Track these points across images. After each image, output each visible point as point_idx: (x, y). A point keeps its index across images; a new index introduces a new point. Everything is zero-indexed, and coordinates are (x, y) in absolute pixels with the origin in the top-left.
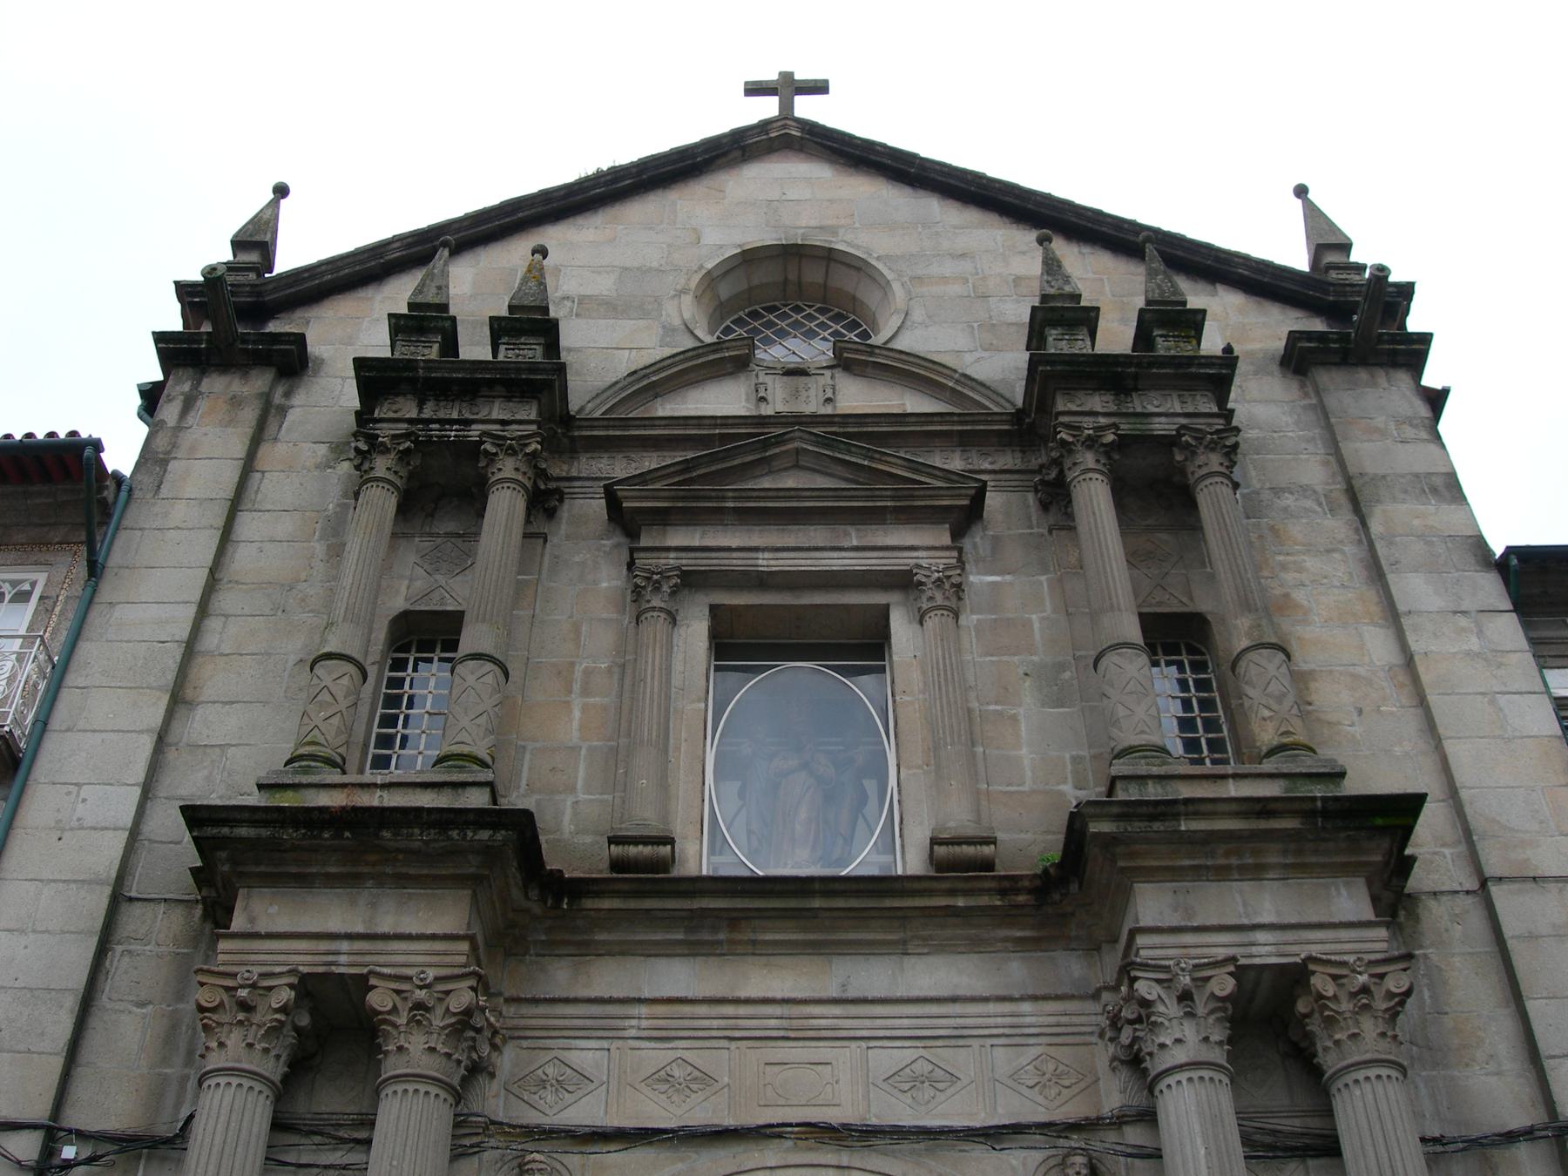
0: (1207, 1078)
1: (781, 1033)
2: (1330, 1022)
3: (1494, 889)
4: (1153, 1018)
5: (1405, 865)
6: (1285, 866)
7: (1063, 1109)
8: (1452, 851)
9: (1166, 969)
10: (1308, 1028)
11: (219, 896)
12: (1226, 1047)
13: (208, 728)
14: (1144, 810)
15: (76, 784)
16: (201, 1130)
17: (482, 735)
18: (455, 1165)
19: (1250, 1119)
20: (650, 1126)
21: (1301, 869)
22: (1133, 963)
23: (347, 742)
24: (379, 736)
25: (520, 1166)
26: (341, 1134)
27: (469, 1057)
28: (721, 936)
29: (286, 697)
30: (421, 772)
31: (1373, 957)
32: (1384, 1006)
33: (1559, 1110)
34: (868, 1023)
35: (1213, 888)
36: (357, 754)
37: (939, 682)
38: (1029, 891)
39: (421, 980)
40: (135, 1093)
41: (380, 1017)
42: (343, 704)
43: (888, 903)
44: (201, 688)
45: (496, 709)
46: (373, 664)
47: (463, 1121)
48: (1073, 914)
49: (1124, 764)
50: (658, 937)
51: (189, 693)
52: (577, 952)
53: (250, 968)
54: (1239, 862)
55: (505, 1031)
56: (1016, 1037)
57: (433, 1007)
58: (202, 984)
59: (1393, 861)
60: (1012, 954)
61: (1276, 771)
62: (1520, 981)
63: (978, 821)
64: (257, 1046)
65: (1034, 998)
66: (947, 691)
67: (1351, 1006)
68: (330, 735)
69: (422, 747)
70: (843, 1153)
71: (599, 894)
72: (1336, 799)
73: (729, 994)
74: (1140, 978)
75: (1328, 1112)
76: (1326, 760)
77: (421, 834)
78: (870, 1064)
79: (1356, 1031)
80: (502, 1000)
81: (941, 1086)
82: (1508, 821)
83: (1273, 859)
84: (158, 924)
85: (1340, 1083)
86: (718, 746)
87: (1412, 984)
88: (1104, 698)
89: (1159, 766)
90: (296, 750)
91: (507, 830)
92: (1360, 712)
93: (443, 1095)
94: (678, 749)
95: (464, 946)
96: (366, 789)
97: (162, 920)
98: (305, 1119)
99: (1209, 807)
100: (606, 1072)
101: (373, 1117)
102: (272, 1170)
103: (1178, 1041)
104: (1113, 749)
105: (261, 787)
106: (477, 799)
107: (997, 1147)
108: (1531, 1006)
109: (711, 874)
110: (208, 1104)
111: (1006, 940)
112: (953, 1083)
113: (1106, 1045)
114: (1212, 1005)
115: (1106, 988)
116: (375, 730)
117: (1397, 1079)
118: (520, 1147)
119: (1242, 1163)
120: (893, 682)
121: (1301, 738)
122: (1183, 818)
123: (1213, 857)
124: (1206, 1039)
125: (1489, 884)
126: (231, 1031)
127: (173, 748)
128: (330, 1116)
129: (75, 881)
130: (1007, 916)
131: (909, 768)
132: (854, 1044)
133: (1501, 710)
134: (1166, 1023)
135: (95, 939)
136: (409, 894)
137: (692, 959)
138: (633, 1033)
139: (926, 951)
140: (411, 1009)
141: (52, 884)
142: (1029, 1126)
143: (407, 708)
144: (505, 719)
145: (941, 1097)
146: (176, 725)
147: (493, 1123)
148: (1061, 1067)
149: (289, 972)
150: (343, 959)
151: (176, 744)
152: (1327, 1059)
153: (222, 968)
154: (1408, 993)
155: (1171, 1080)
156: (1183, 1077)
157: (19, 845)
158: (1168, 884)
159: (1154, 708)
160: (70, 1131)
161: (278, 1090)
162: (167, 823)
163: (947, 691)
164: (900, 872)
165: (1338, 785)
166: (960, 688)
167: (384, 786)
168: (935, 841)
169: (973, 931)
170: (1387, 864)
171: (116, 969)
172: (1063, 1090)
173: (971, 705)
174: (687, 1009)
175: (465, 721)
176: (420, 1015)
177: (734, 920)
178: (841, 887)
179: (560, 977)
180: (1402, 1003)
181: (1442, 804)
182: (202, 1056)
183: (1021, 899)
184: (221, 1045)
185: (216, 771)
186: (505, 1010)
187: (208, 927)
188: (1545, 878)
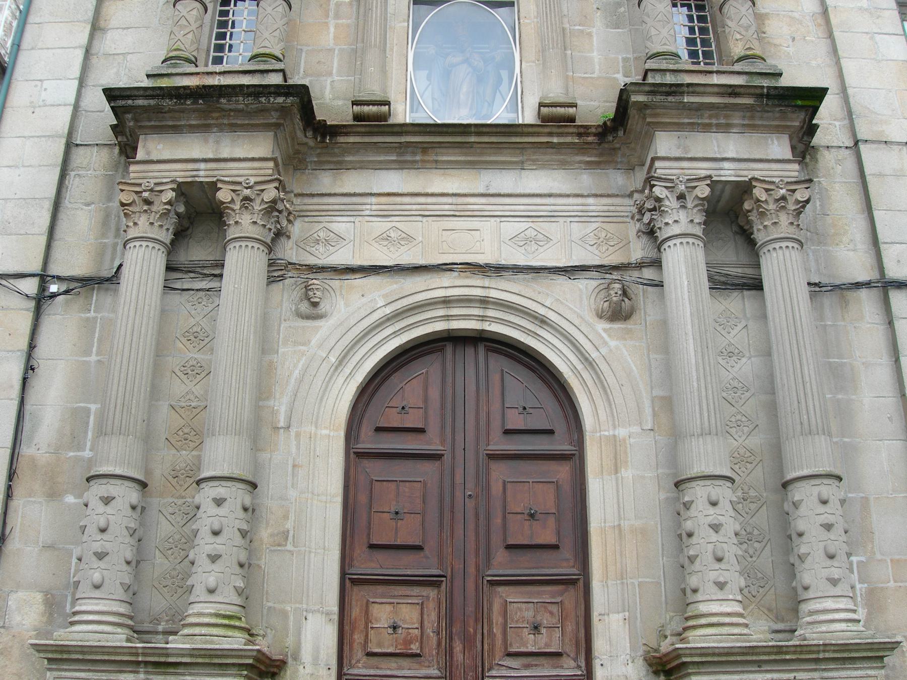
0: (691, 243)
1: (452, 213)
2: (762, 215)
3: (862, 147)
4: (662, 208)
5: (812, 130)
6: (744, 125)
7: (610, 258)
8: (839, 123)
9: (671, 181)
10: (749, 218)
11: (128, 140)
12: (703, 226)
13: (115, 44)
14: (664, 89)
15: (40, 80)
16: (127, 272)
17: (277, 42)
18: (270, 286)
19: (713, 267)
20: (378, 264)
21: (753, 128)
22: (653, 177)
23: (198, 49)
24: (216, 45)
25: (306, 287)
26: (205, 272)
27: (275, 227)
28: (418, 158)
29: (160, 24)
30: (242, 64)
31: (789, 180)
32: (794, 208)
33: (886, 272)
34: (501, 207)
35: (700, 136)
36: (204, 55)
37: (546, 12)
38: (595, 135)
39: (247, 184)
40: (88, 254)
41: (224, 205)
42: (194, 26)
43: (514, 139)
44: (109, 20)
45: (285, 27)
46: (210, 2)
47: (274, 263)
48: (619, 149)
49: (653, 62)
50: (382, 158)
51: (102, 24)
52: (335, 168)
53: (149, 180)
54: (717, 122)
55: (295, 213)
56: (584, 217)
57: (254, 199)
58: (122, 191)
59: (805, 126)
60: (583, 171)
61: (742, 71)
62: (871, 200)
63: (567, 94)
64: (155, 224)
65: (596, 196)
66: (551, 17)
67: (775, 207)
68: (188, 47)
69: (241, 51)
70: (485, 279)
71: (347, 134)
72: (776, 88)
73: (422, 191)
74: (656, 185)
75: (758, 266)
76: (771, 66)
77: (243, 100)
78: (502, 231)
79: (777, 221)
80: (293, 195)
81: (541, 243)
82: (874, 108)
83: (736, 121)
84: (94, 158)
85: (765, 250)
86: (415, 48)
87: (810, 196)
88: (643, 24)
89: (674, 64)
90: (168, 54)
91: (293, 97)
92: (794, 39)
93: (262, 248)
94: (392, 50)
95: (271, 164)
96: (210, 75)
97: (96, 156)
98: (184, 264)
99: (701, 89)
100: (353, 235)
101: (222, 262)
102: (168, 293)
103: (676, 221)
104: (647, 54)
105: (148, 76)
106: (275, 79)
107: (572, 278)
108: (876, 214)
109: (411, 122)
110: (130, 257)
111: (580, 162)
112: (548, 242)
113: (635, 223)
114: (696, 202)
115: (637, 191)
116: (213, 41)
117: (797, 248)
118: (305, 277)
119: (708, 290)
120: (519, 11)
121: (758, 52)
122: (686, 94)
123: (701, 118)
124: (692, 221)
125: (860, 143)
126: (140, 216)
127: (95, 57)
128: (198, 262)
129: (44, 136)
130: (581, 149)
131: (527, 62)
132: (493, 219)
133: (876, 43)
134: (670, 211)
135: (59, 169)
136: (238, 135)
137: (401, 171)
138: (368, 213)
139: (534, 167)
140: (242, 201)
141: (31, 139)
142: (590, 267)
143: (232, 28)
144: (290, 33)
145: (541, 249)
146: (96, 43)
147: (291, 264)
148: (609, 235)
149: (171, 181)
150: (202, 173)
151: (97, 54)
152: (759, 235)
153: (132, 181)
154: (808, 201)
155: (671, 243)
156: (678, 241)
157: (9, 115)
158: (675, 133)
159: (672, 30)
160: (53, 277)
161: (170, 249)
162: (96, 101)
163: (551, 17)
164: (520, 122)
165: (777, 81)
166: (558, 15)
167: (220, 73)
168: (541, 105)
169: (562, 157)
170: (802, 127)
171: (72, 185)
172: (609, 247)
173: (564, 26)
174: (398, 199)
175: (266, 34)
176: (247, 203)
177: (425, 148)
178: (487, 130)
179: (326, 181)
180: (804, 207)
181: (837, 96)
182: (125, 231)
183: (590, 139)
184: (135, 224)
185: (121, 68)
186: (295, 200)
187: (123, 158)
188: (892, 143)
